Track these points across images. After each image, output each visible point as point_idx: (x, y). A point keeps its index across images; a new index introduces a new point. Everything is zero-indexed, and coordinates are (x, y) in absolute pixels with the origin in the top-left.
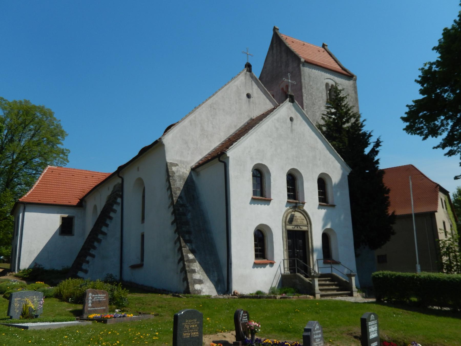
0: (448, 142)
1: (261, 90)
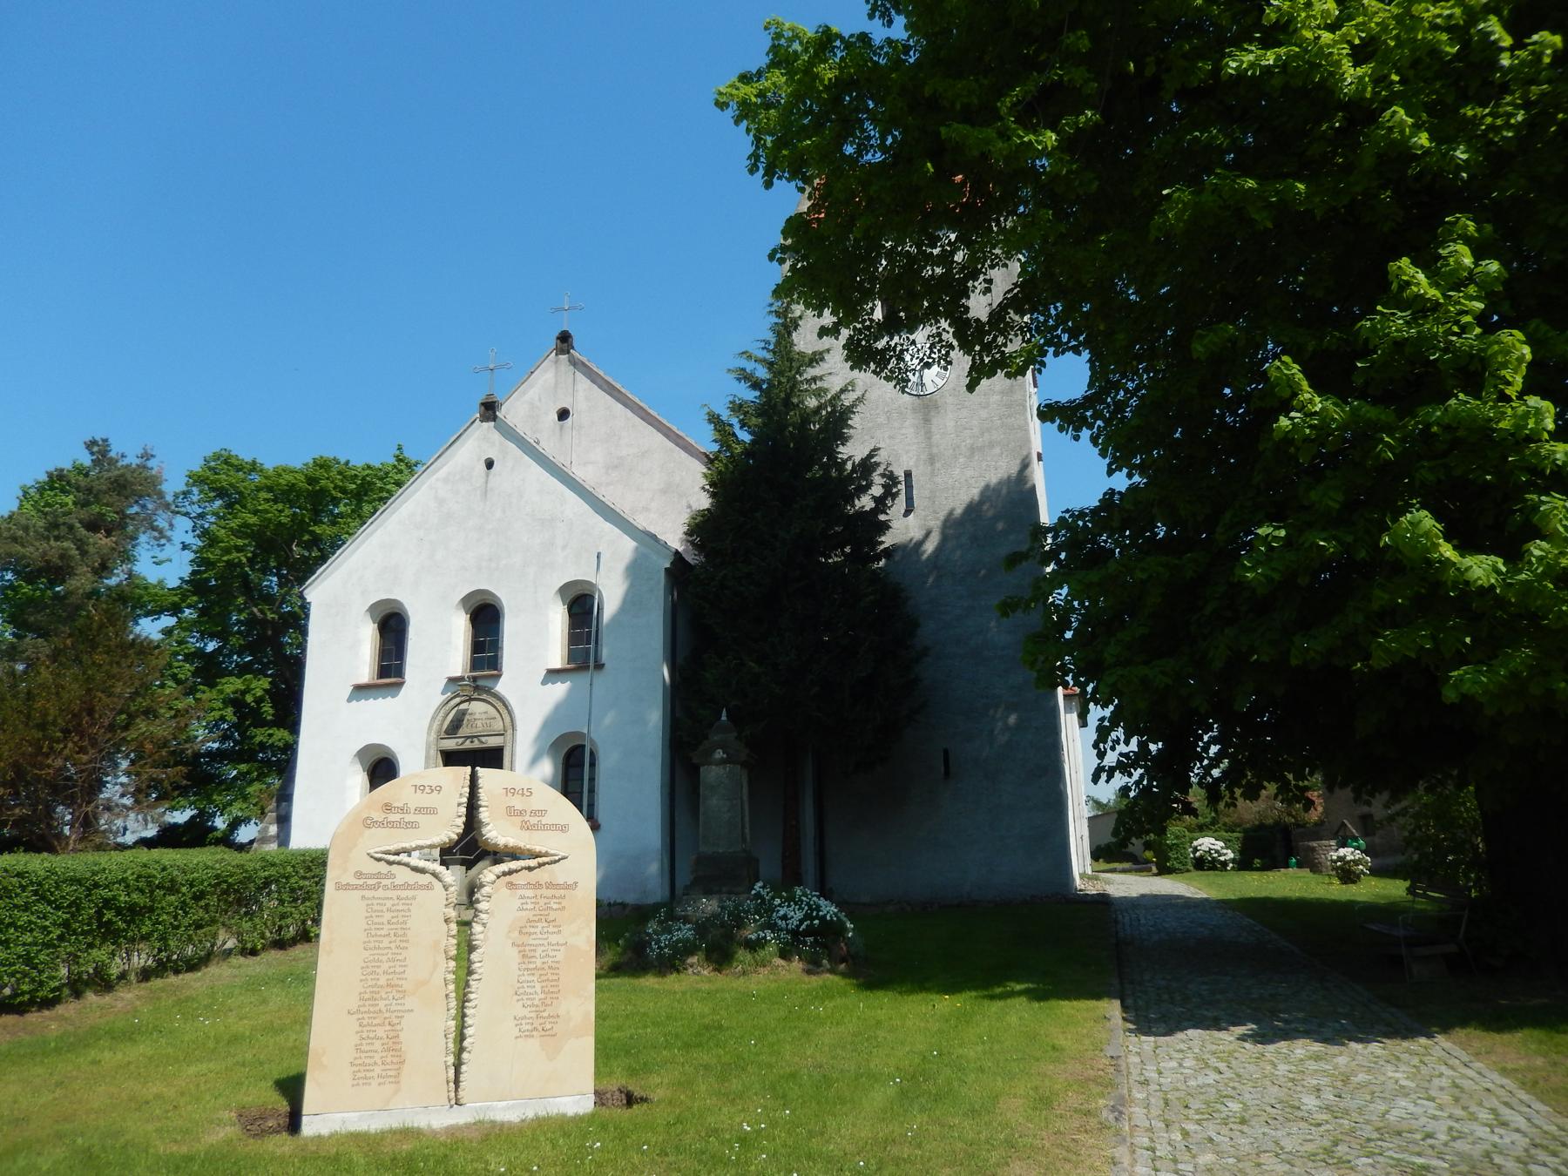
1: (600, 387)
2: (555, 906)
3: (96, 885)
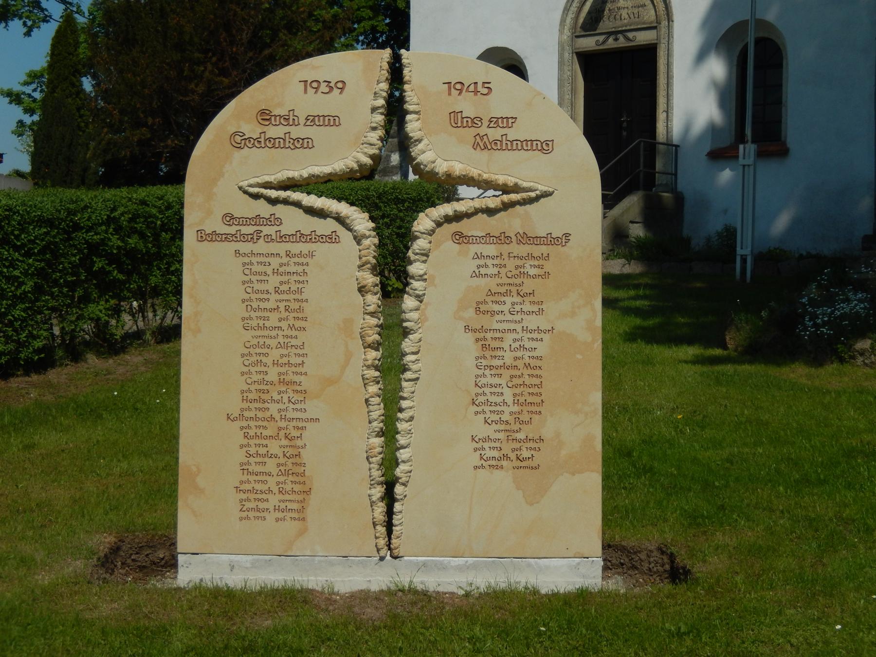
0: (166, 341)
2: (533, 271)
3: (77, 227)
